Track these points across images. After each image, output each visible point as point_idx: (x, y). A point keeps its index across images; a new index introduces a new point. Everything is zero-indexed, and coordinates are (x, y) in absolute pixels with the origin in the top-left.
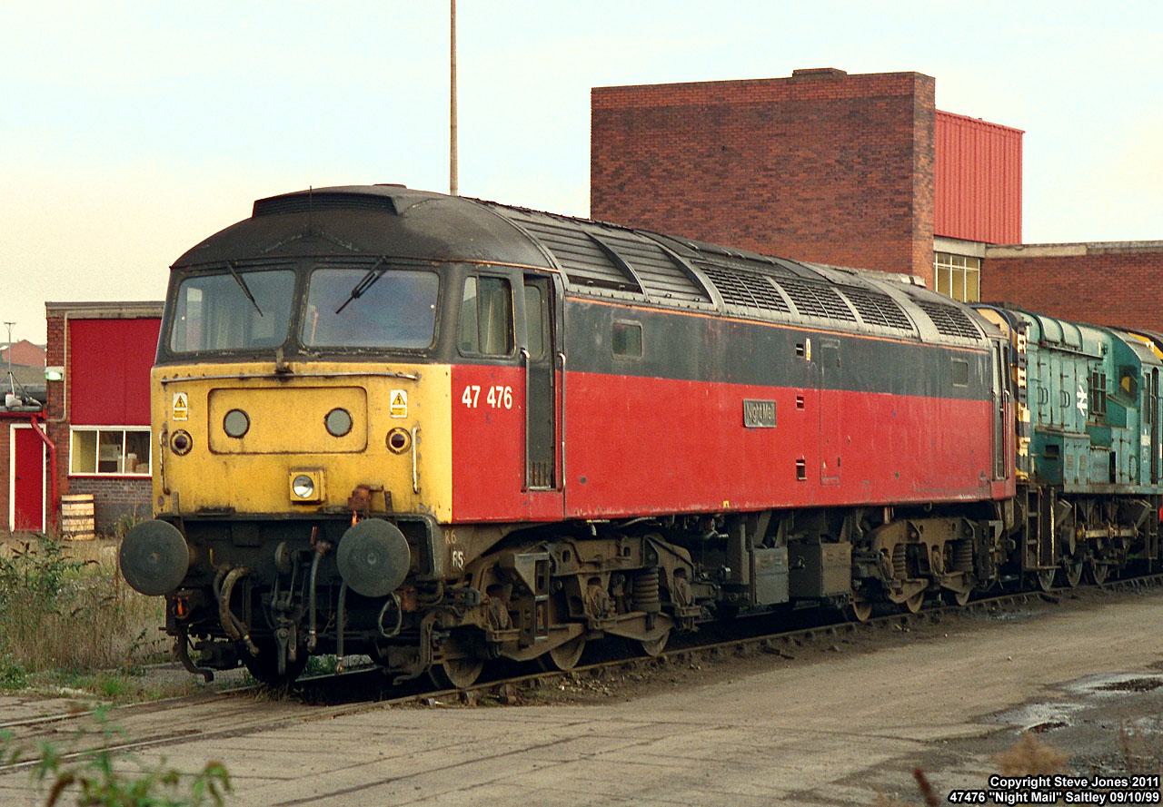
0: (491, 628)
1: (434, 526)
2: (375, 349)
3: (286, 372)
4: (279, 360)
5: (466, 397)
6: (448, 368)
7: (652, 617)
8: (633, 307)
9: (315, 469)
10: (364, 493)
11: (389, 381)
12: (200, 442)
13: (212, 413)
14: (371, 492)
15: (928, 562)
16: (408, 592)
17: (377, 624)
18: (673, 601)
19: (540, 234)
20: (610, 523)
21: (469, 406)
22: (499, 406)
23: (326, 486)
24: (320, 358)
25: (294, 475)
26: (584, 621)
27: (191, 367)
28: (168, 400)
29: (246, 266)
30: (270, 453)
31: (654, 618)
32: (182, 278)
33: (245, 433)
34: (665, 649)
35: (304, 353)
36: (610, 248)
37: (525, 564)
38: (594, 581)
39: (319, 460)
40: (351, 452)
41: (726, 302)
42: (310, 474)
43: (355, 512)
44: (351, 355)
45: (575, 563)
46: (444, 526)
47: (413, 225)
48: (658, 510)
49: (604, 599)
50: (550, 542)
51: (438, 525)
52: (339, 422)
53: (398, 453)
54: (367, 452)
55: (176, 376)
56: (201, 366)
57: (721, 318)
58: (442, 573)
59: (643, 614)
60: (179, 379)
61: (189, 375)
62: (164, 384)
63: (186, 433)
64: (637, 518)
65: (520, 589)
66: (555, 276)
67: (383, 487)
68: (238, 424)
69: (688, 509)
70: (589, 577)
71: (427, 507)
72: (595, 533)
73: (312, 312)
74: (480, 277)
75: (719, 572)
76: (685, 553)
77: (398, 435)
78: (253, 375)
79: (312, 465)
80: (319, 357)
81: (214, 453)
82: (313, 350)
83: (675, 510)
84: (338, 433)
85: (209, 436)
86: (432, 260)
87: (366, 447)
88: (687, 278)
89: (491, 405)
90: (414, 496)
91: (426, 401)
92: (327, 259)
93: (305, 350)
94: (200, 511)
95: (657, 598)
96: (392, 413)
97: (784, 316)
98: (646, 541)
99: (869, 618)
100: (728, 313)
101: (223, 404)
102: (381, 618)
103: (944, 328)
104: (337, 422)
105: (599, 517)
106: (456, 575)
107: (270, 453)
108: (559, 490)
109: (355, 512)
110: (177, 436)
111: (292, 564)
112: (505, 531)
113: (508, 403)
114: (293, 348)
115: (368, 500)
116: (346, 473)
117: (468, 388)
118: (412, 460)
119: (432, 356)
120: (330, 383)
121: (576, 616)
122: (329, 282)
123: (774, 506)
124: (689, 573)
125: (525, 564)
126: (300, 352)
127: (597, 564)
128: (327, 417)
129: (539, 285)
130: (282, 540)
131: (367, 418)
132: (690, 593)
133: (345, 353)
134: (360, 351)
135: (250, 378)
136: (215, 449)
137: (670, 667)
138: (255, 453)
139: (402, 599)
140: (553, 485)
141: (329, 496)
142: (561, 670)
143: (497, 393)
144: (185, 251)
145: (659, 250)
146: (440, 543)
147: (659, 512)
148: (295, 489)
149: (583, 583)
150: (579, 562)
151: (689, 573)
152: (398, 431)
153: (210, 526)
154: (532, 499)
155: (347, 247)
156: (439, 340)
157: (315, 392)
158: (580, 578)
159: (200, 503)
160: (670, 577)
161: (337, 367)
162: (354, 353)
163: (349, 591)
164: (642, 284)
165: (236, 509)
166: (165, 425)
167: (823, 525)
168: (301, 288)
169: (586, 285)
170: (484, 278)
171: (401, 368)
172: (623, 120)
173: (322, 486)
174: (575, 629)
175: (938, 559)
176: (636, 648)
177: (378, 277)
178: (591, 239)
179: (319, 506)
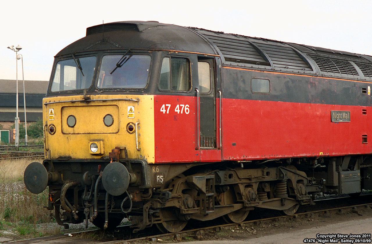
0: (183, 208)
1: (145, 165)
2: (124, 89)
3: (88, 99)
4: (84, 94)
5: (177, 109)
6: (152, 96)
7: (283, 200)
8: (265, 72)
9: (99, 140)
10: (116, 150)
11: (127, 102)
12: (58, 129)
13: (63, 117)
14: (121, 150)
16: (136, 193)
17: (120, 206)
18: (296, 193)
19: (258, 44)
20: (252, 162)
21: (178, 113)
22: (182, 113)
23: (104, 148)
24: (102, 93)
25: (91, 143)
26: (242, 203)
27: (55, 98)
28: (47, 111)
29: (79, 55)
30: (83, 134)
31: (285, 201)
32: (57, 61)
33: (74, 125)
34: (296, 213)
35: (97, 91)
36: (259, 48)
37: (199, 181)
38: (248, 186)
39: (101, 137)
40: (113, 133)
41: (321, 71)
42: (96, 142)
43: (112, 159)
44: (114, 91)
45: (237, 179)
46: (151, 165)
47: (144, 36)
48: (280, 156)
49: (252, 194)
50: (221, 170)
51: (148, 164)
52: (108, 120)
53: (131, 133)
54: (119, 133)
55: (50, 101)
56: (59, 97)
57: (318, 77)
58: (150, 185)
59: (280, 199)
60: (51, 103)
61: (54, 101)
62: (46, 105)
63: (53, 125)
64: (266, 160)
65: (200, 192)
66: (216, 58)
67: (125, 148)
68: (72, 122)
69: (299, 156)
70: (245, 185)
71: (143, 156)
72: (242, 166)
73: (102, 73)
74: (171, 57)
75: (321, 181)
76: (303, 174)
77: (131, 126)
78: (76, 101)
79: (99, 139)
80: (102, 93)
81: (64, 133)
82: (101, 90)
83: (291, 156)
84: (109, 125)
85: (62, 127)
86: (149, 50)
87: (118, 131)
88: (303, 61)
89: (177, 112)
90: (138, 152)
91: (143, 110)
92: (109, 51)
93: (97, 90)
94: (59, 158)
96: (128, 116)
98: (279, 169)
100: (322, 75)
101: (68, 112)
102: (122, 204)
104: (108, 121)
105: (244, 160)
106: (160, 186)
107: (83, 134)
108: (219, 149)
109: (112, 159)
110: (50, 126)
111: (92, 181)
112: (189, 167)
113: (187, 112)
114: (93, 90)
115: (119, 154)
116: (113, 141)
118: (136, 136)
119: (146, 91)
120: (105, 104)
122: (109, 60)
123: (349, 154)
124: (305, 182)
125: (199, 181)
126: (96, 91)
127: (250, 179)
128: (104, 118)
129: (209, 61)
130: (86, 171)
131: (119, 119)
132: (304, 189)
133: (112, 91)
134: (118, 90)
135: (76, 102)
136: (64, 132)
137: (299, 220)
138: (78, 134)
139: (133, 196)
140: (215, 147)
141: (106, 152)
142: (288, 215)
143: (180, 108)
144: (62, 49)
146: (146, 170)
147: (281, 157)
148: (91, 149)
149: (242, 188)
150: (239, 178)
151: (305, 182)
152: (131, 124)
153: (63, 164)
154: (202, 152)
155: (117, 46)
156: (149, 85)
157: (100, 107)
159: (59, 155)
160: (294, 184)
161: (107, 96)
162: (116, 91)
164: (271, 62)
165: (72, 157)
166: (46, 122)
167: (346, 163)
168: (98, 64)
169: (236, 62)
170: (173, 57)
171: (132, 97)
173: (102, 147)
174: (237, 207)
176: (282, 213)
177: (128, 59)
178: (251, 44)
179: (102, 156)
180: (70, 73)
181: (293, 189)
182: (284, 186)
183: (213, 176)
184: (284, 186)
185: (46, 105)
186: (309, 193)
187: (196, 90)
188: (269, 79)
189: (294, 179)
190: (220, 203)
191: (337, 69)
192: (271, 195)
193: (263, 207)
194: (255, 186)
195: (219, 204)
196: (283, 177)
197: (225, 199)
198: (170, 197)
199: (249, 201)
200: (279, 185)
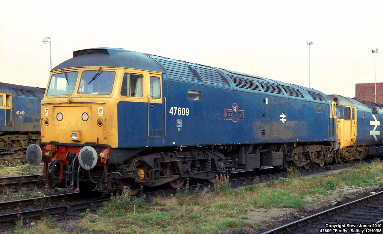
0: (294, 161)
5: (171, 111)
15: (310, 156)
21: (172, 114)
37: (148, 159)
38: (185, 163)
59: (206, 171)
65: (149, 168)
72: (181, 150)
89: (171, 114)
95: (210, 168)
97: (283, 96)
99: (309, 168)
103: (237, 85)
112: (141, 150)
113: (180, 113)
117: (172, 108)
121: (214, 169)
143: (174, 110)
144: (57, 66)
145: (217, 72)
158: (178, 163)
163: (81, 167)
167: (251, 149)
172: (360, 88)
174: (309, 161)
175: (313, 156)
176: (318, 165)
180: (62, 83)
181: (215, 165)
182: (209, 163)
183: (159, 157)
184: (209, 163)
185: (43, 104)
186: (226, 168)
187: (164, 98)
188: (200, 91)
189: (216, 160)
190: (165, 175)
191: (247, 87)
192: (201, 169)
193: (195, 177)
194: (190, 163)
195: (164, 176)
196: (209, 157)
197: (168, 172)
198: (127, 171)
199: (184, 173)
200: (207, 163)
